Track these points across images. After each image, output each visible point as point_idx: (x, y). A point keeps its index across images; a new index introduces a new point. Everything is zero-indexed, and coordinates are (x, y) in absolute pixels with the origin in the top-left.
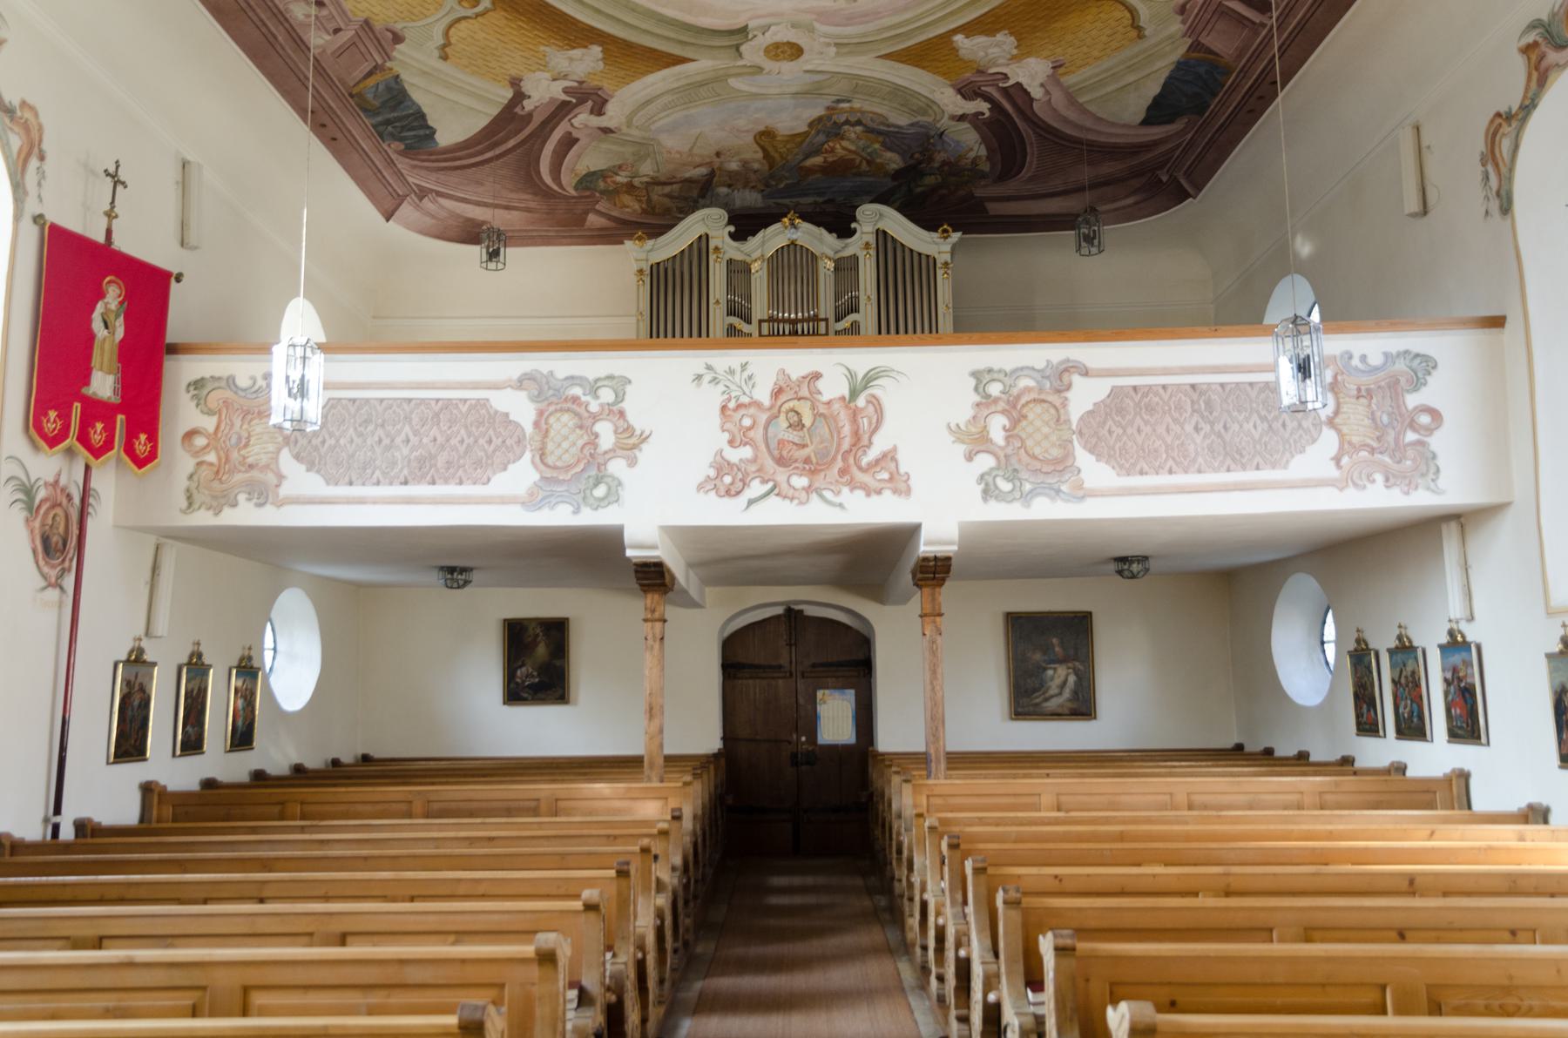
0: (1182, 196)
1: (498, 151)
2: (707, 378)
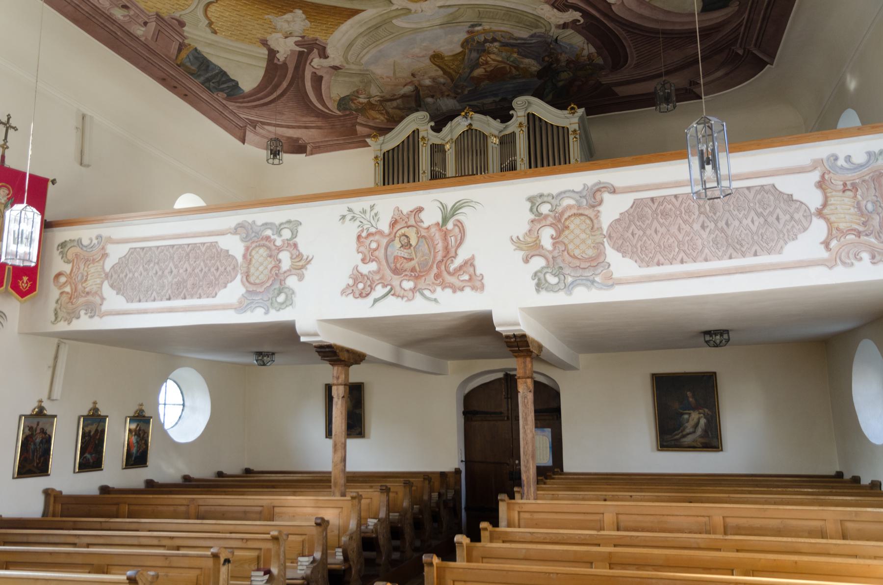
0: (759, 65)
1: (279, 92)
2: (349, 217)
